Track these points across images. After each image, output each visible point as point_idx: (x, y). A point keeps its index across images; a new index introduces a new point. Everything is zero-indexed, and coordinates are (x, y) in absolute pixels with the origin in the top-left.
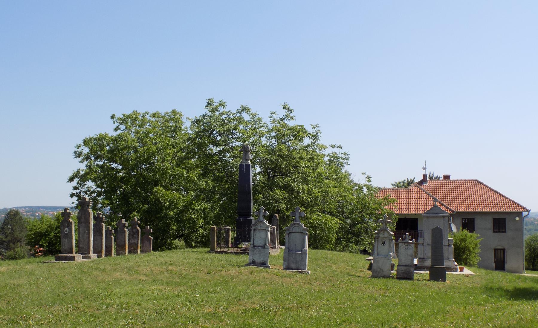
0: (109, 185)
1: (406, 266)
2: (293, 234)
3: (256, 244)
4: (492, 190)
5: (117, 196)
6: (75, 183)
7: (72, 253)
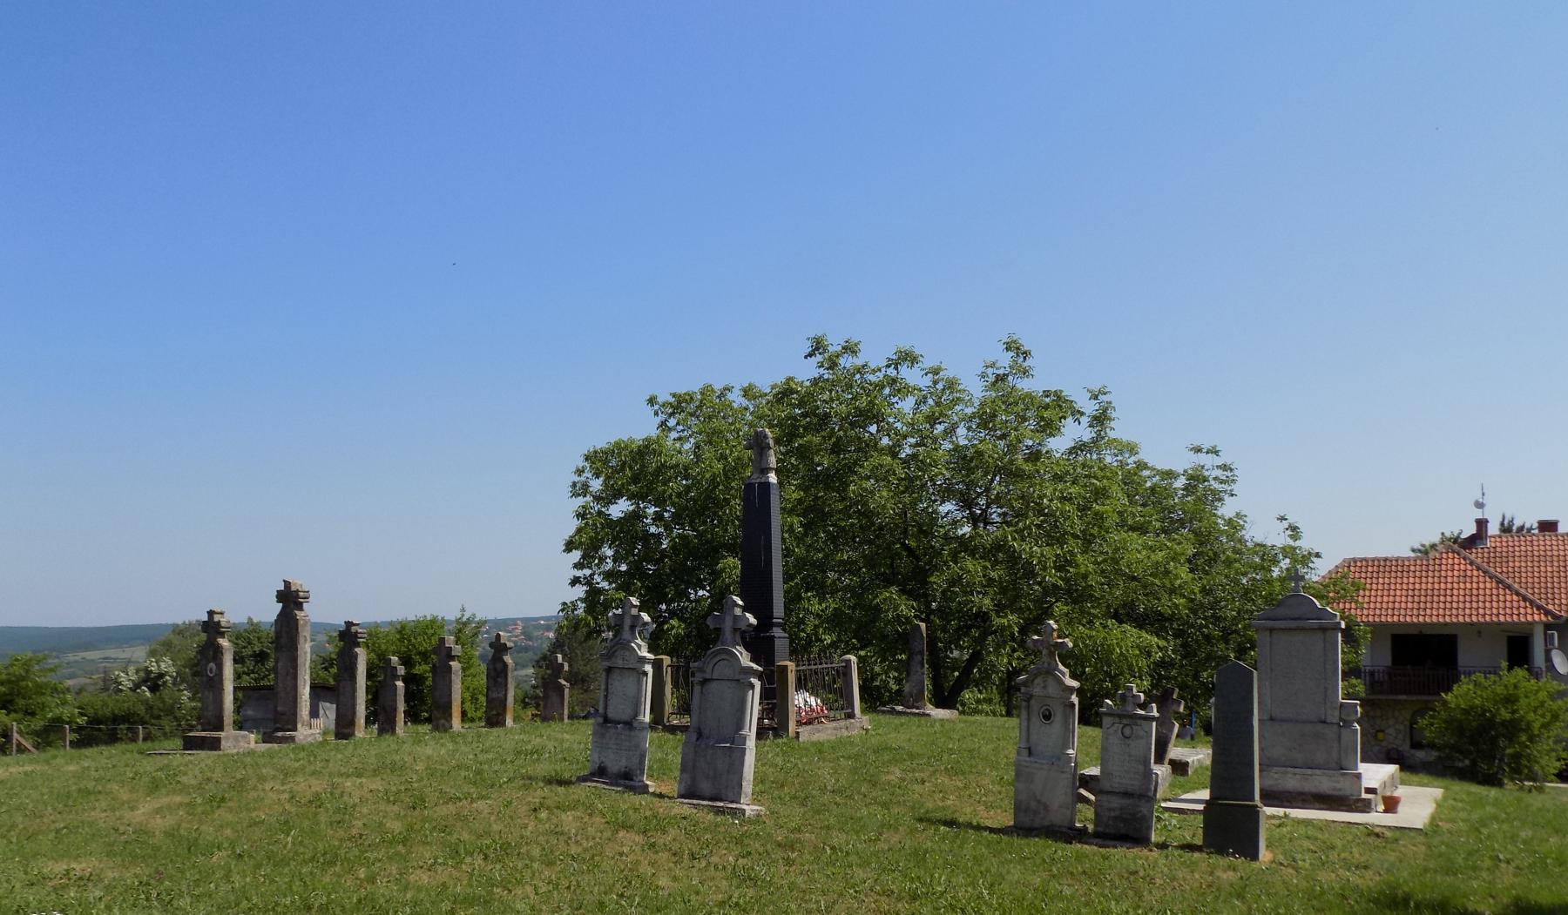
2: (714, 685)
3: (612, 714)
7: (220, 728)
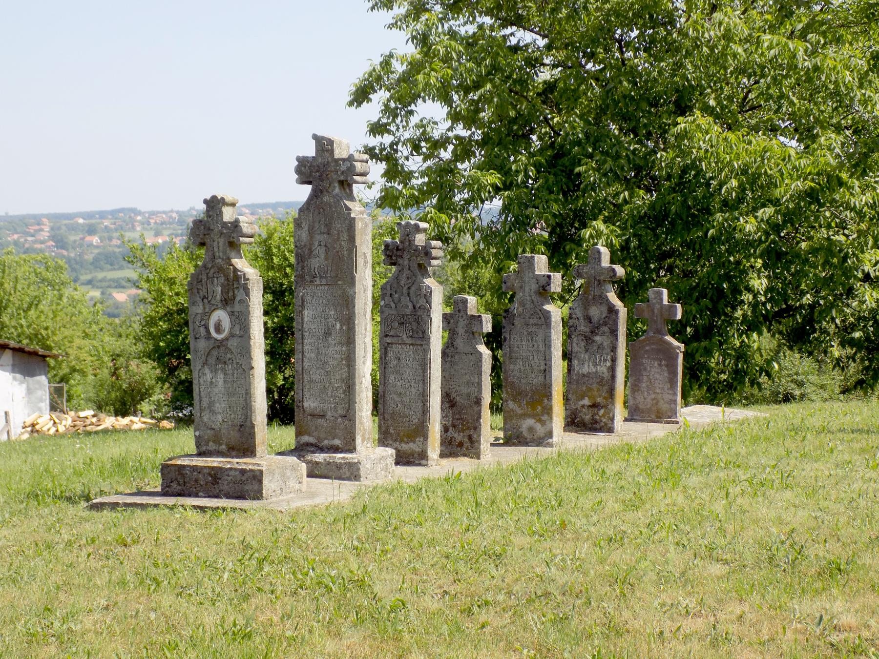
0: (500, 116)
5: (532, 155)
6: (373, 110)
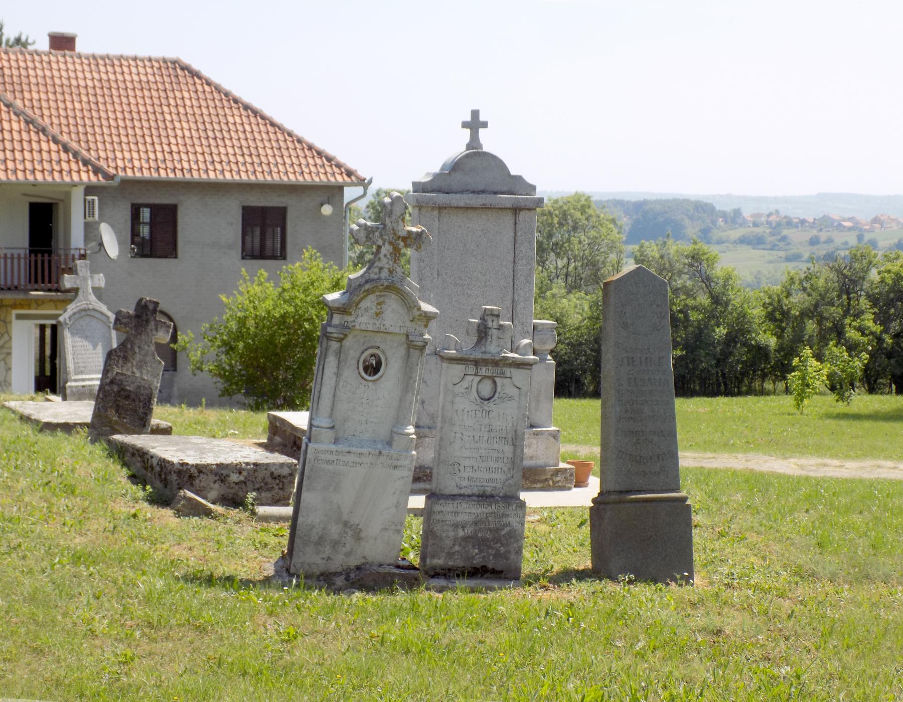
1: (484, 497)
4: (236, 101)
